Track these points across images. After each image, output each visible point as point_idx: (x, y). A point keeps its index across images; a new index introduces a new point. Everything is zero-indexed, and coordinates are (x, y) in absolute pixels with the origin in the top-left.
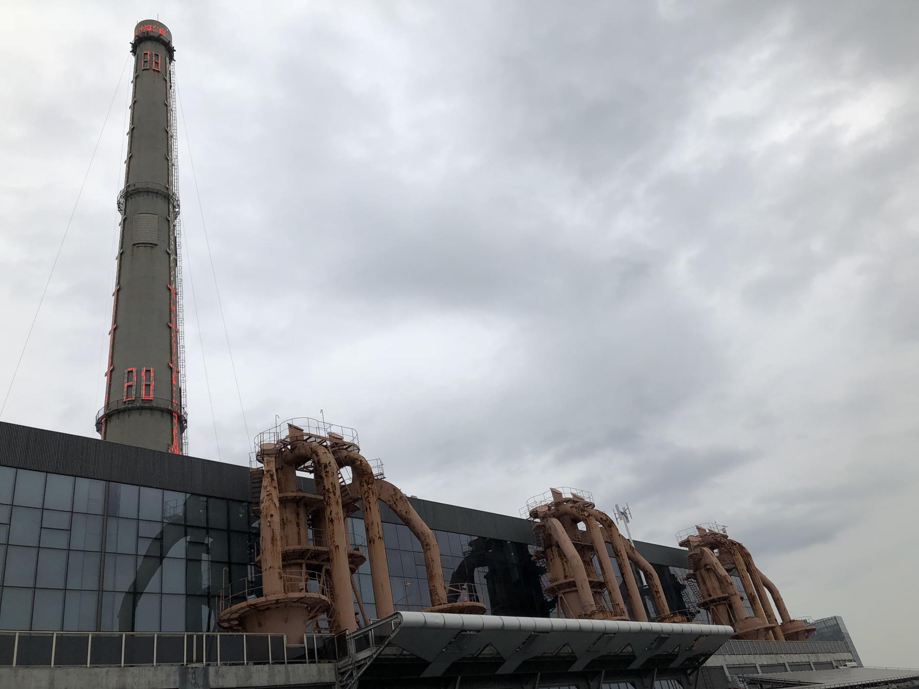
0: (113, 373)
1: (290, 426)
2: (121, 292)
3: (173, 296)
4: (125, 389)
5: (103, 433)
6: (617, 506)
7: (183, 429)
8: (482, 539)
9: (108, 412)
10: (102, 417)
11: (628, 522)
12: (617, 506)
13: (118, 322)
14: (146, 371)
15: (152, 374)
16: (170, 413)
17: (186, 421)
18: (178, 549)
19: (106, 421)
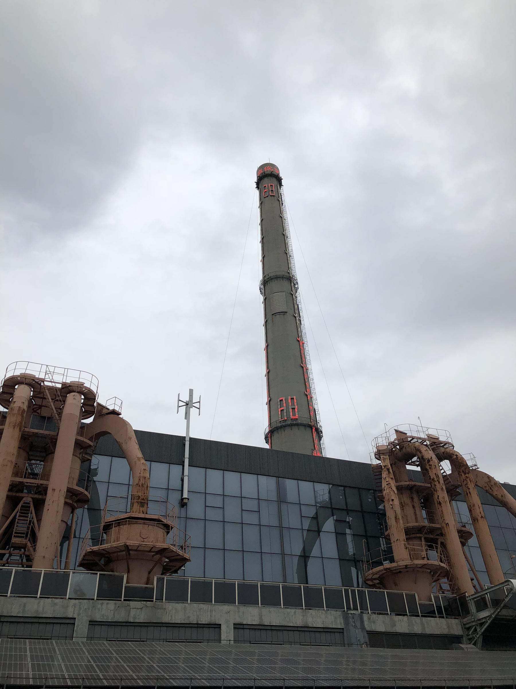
0: (271, 402)
7: (320, 438)
15: (295, 400)
16: (311, 427)
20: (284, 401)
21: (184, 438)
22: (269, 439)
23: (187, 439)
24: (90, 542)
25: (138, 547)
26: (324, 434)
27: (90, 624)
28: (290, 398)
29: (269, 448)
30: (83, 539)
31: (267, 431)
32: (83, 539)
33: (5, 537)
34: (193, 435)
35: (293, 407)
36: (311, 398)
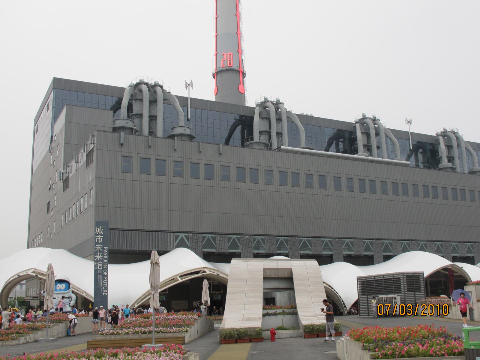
0: (217, 18)
1: (265, 98)
2: (218, 36)
3: (238, 18)
4: (222, 62)
5: (215, 79)
6: (407, 118)
7: (244, 77)
8: (338, 129)
9: (216, 71)
10: (215, 73)
11: (410, 125)
12: (407, 118)
13: (218, 15)
14: (229, 54)
15: (232, 56)
16: (239, 72)
17: (245, 74)
18: (239, 128)
19: (216, 75)
20: (225, 56)
21: (188, 98)
22: (215, 76)
23: (189, 98)
24: (417, 293)
25: (345, 250)
26: (246, 75)
27: (150, 339)
28: (228, 54)
29: (214, 100)
30: (424, 313)
31: (214, 72)
32: (424, 313)
33: (91, 174)
34: (191, 97)
35: (230, 59)
36: (239, 17)
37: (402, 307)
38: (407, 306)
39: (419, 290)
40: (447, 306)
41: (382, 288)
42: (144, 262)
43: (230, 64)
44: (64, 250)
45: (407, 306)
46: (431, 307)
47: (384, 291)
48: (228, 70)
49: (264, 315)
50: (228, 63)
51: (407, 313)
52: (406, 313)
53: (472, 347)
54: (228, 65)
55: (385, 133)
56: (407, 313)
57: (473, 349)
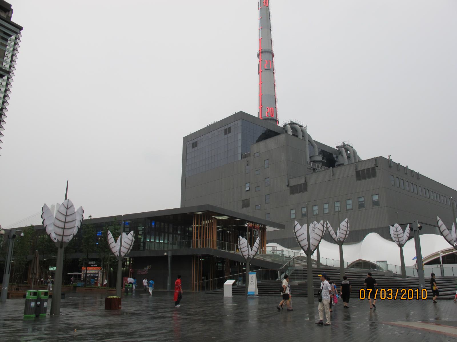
37: (410, 292)
38: (388, 291)
39: (241, 276)
40: (426, 290)
41: (304, 274)
42: (411, 239)
43: (272, 115)
44: (371, 233)
45: (388, 291)
46: (411, 292)
47: (295, 276)
48: (271, 119)
49: (62, 288)
50: (271, 115)
51: (388, 297)
52: (386, 298)
53: (31, 298)
54: (271, 116)
55: (308, 141)
56: (388, 297)
57: (30, 299)
